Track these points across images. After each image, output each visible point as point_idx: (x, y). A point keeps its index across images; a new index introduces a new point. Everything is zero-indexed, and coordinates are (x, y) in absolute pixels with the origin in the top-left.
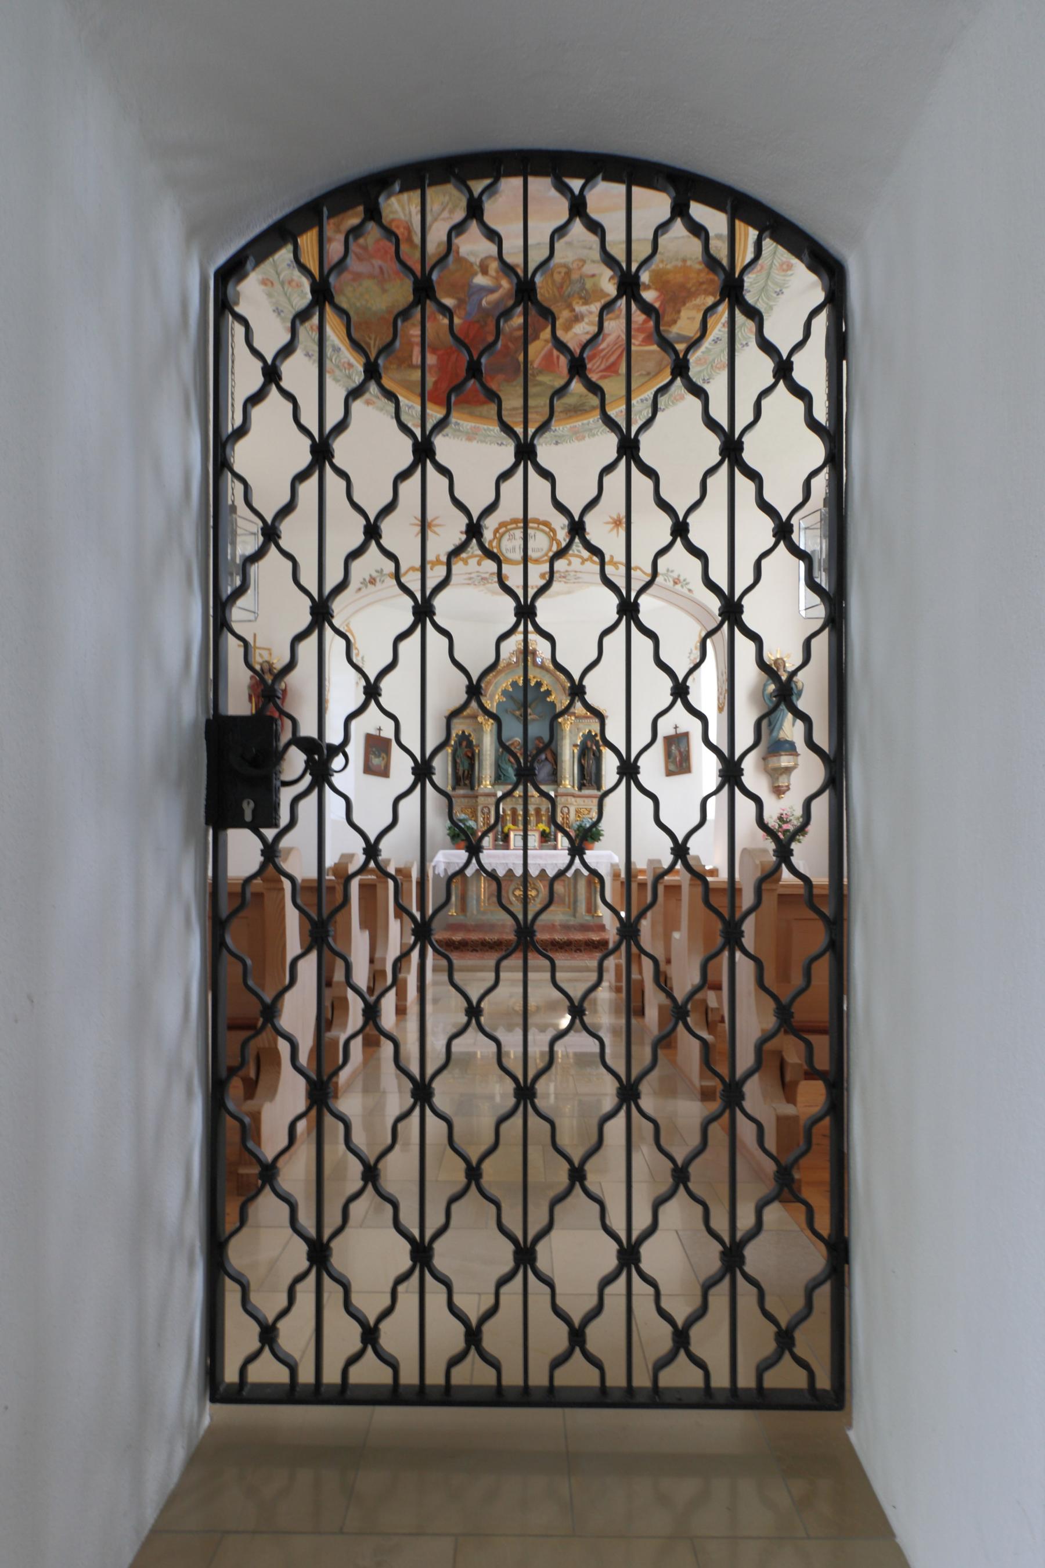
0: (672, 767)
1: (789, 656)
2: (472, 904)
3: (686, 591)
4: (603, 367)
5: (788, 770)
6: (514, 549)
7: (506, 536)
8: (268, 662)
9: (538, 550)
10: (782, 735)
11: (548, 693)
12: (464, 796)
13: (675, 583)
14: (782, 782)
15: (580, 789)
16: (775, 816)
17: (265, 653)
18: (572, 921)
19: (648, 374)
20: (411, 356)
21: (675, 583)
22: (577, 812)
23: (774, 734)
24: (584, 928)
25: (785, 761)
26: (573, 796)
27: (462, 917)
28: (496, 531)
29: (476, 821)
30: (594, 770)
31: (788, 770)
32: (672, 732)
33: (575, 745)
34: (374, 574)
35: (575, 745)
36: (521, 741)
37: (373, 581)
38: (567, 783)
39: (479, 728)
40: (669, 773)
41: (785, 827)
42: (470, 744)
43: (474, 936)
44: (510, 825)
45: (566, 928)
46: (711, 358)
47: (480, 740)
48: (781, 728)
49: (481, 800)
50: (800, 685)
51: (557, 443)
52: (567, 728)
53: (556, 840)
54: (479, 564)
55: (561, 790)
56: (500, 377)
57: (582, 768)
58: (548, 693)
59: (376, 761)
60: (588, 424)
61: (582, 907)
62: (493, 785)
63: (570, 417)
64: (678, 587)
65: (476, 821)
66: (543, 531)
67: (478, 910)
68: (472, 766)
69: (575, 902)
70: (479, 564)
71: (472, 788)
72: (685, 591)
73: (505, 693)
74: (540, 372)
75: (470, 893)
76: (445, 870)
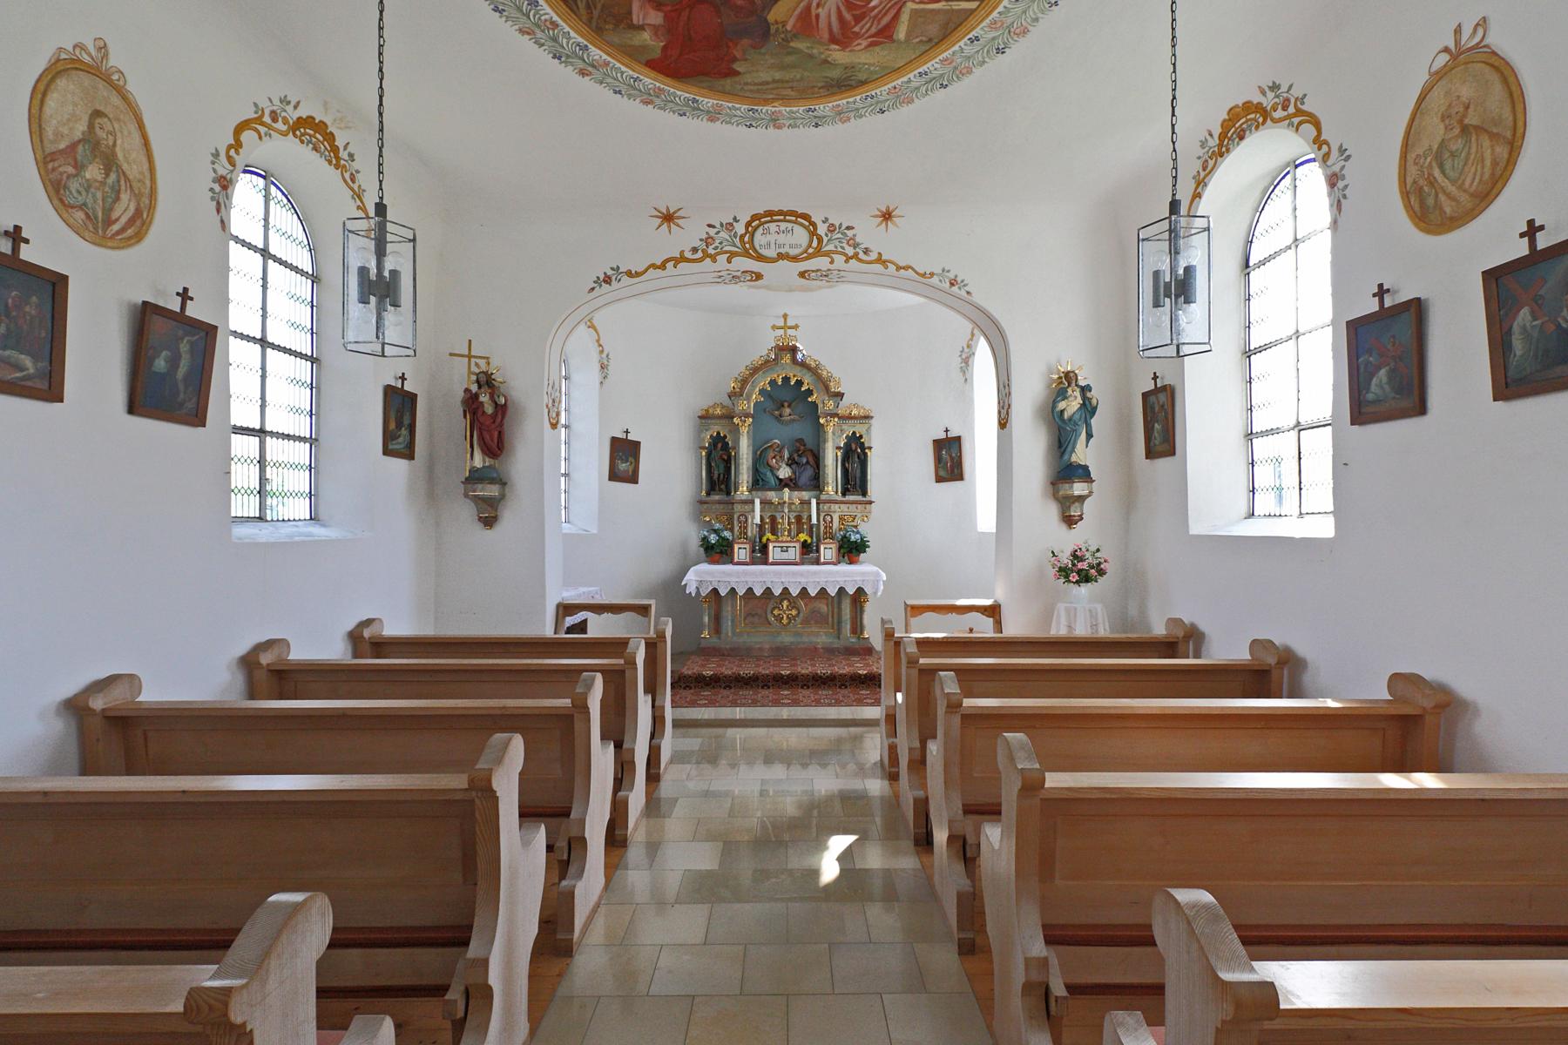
0: (942, 473)
1: (1080, 368)
2: (727, 625)
3: (963, 293)
4: (873, 30)
5: (1081, 499)
6: (769, 244)
7: (760, 230)
8: (485, 373)
9: (797, 246)
10: (1074, 458)
11: (809, 392)
12: (719, 502)
13: (952, 284)
14: (1074, 512)
15: (844, 494)
16: (1068, 553)
17: (482, 363)
18: (837, 644)
19: (930, 40)
20: (630, 13)
21: (952, 284)
22: (841, 518)
23: (1066, 457)
24: (850, 652)
25: (1079, 488)
26: (836, 502)
27: (715, 640)
28: (748, 224)
29: (732, 530)
30: (858, 474)
31: (1081, 499)
32: (943, 436)
33: (839, 448)
34: (610, 273)
35: (839, 448)
36: (781, 445)
37: (608, 280)
38: (830, 489)
39: (735, 430)
40: (939, 479)
41: (1080, 566)
42: (725, 446)
43: (728, 669)
44: (769, 535)
45: (830, 652)
46: (1009, 21)
47: (737, 441)
48: (1073, 450)
49: (738, 508)
50: (1094, 402)
51: (817, 125)
52: (830, 430)
53: (818, 551)
54: (729, 261)
55: (823, 497)
56: (745, 42)
57: (845, 472)
58: (809, 392)
59: (623, 466)
60: (910, 81)
61: (847, 628)
62: (750, 491)
63: (833, 94)
64: (955, 289)
65: (732, 530)
66: (802, 225)
67: (734, 633)
68: (728, 470)
69: (840, 622)
70: (729, 261)
71: (728, 493)
72: (963, 293)
73: (762, 392)
74: (795, 36)
75: (724, 614)
76: (698, 592)
